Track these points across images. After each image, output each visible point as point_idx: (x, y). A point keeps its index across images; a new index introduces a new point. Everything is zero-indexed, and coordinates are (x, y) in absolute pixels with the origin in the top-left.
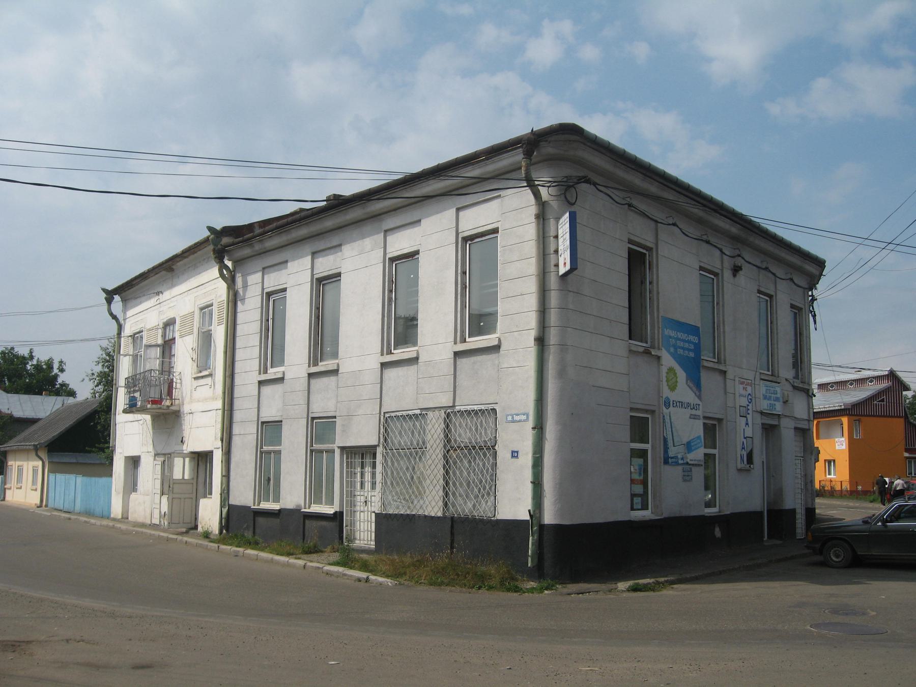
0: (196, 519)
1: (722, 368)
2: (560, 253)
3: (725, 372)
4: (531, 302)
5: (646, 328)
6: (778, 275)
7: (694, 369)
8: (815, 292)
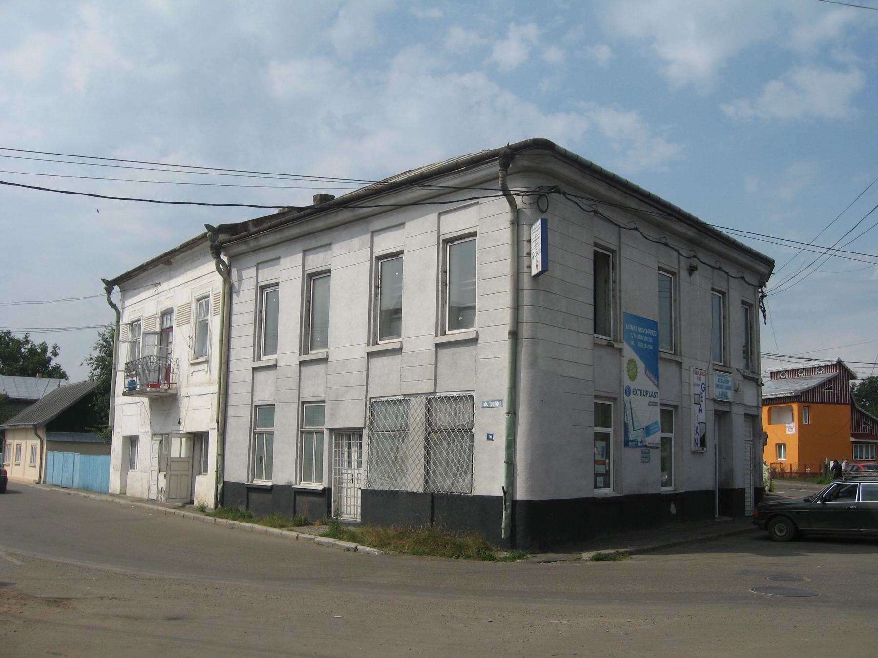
0: (192, 494)
1: (678, 359)
2: (532, 255)
3: (681, 363)
4: (506, 300)
5: (609, 323)
6: (730, 274)
7: (652, 360)
8: (764, 289)
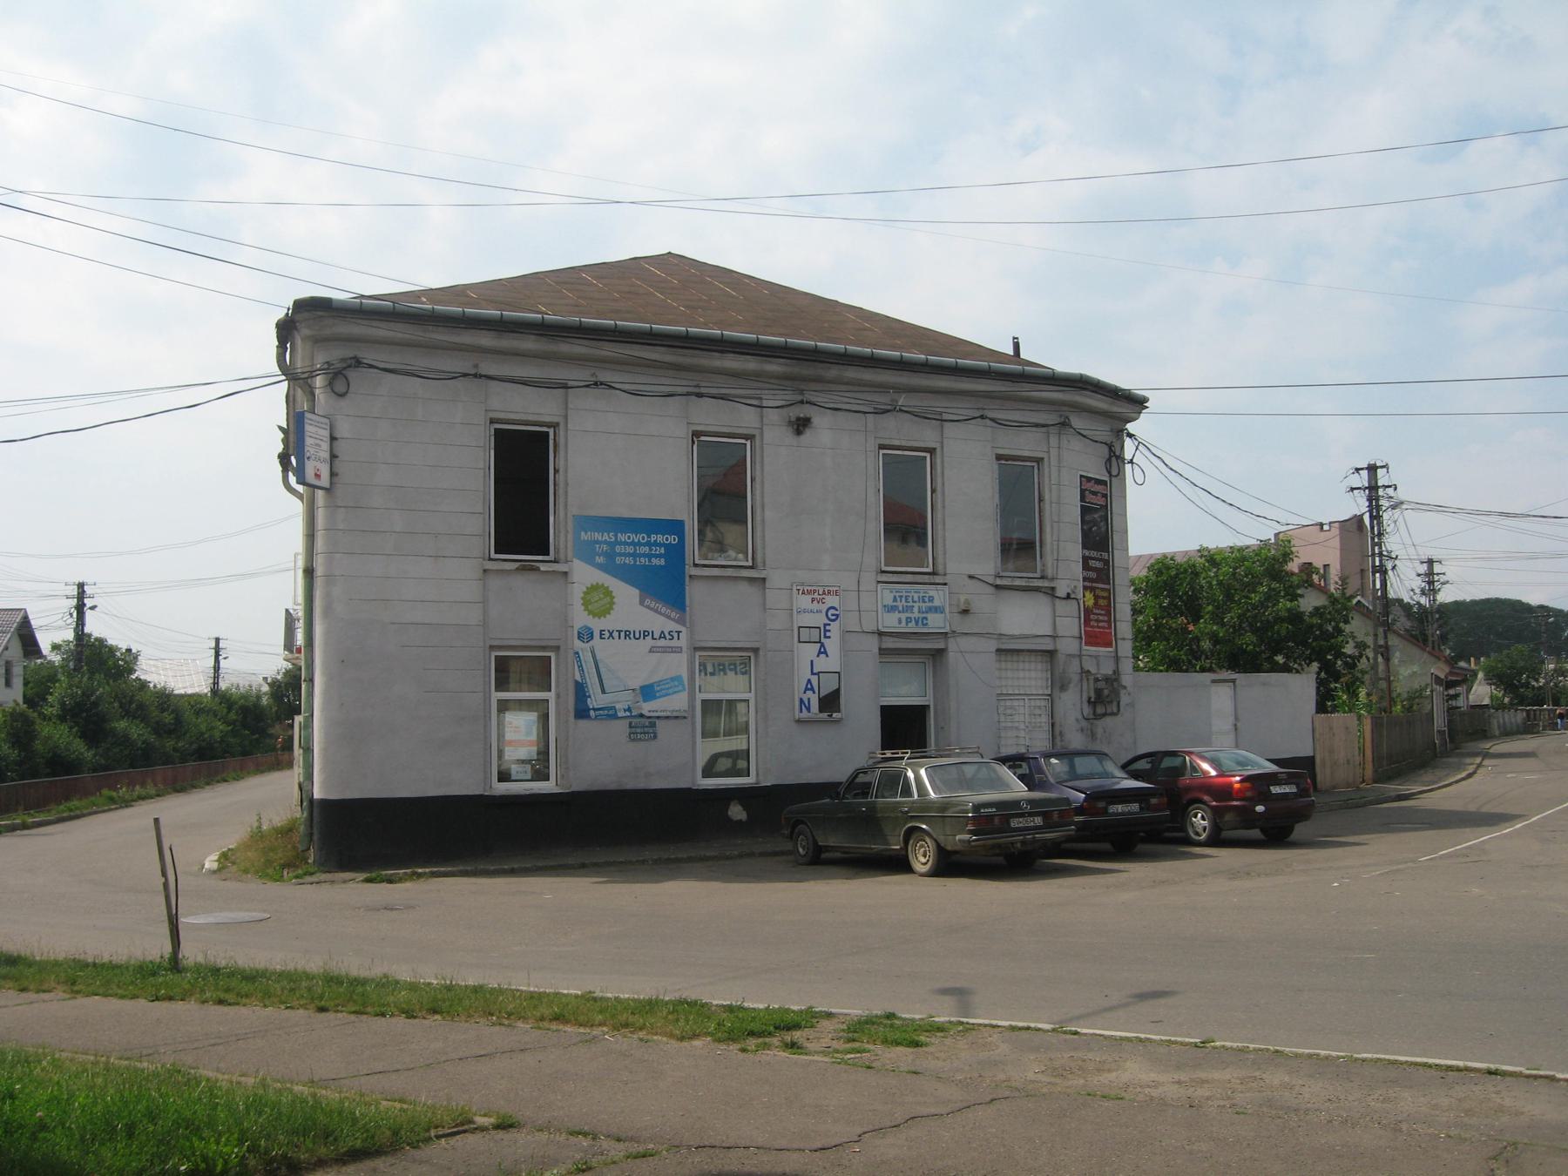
3: (1053, 589)
